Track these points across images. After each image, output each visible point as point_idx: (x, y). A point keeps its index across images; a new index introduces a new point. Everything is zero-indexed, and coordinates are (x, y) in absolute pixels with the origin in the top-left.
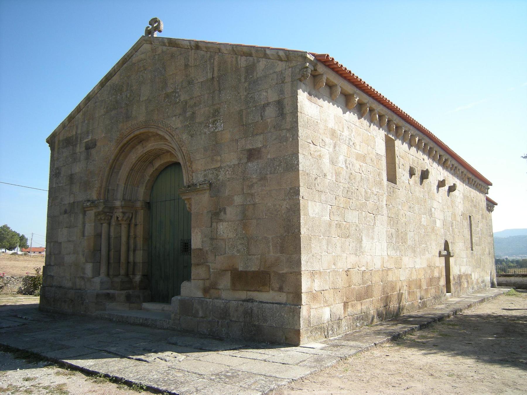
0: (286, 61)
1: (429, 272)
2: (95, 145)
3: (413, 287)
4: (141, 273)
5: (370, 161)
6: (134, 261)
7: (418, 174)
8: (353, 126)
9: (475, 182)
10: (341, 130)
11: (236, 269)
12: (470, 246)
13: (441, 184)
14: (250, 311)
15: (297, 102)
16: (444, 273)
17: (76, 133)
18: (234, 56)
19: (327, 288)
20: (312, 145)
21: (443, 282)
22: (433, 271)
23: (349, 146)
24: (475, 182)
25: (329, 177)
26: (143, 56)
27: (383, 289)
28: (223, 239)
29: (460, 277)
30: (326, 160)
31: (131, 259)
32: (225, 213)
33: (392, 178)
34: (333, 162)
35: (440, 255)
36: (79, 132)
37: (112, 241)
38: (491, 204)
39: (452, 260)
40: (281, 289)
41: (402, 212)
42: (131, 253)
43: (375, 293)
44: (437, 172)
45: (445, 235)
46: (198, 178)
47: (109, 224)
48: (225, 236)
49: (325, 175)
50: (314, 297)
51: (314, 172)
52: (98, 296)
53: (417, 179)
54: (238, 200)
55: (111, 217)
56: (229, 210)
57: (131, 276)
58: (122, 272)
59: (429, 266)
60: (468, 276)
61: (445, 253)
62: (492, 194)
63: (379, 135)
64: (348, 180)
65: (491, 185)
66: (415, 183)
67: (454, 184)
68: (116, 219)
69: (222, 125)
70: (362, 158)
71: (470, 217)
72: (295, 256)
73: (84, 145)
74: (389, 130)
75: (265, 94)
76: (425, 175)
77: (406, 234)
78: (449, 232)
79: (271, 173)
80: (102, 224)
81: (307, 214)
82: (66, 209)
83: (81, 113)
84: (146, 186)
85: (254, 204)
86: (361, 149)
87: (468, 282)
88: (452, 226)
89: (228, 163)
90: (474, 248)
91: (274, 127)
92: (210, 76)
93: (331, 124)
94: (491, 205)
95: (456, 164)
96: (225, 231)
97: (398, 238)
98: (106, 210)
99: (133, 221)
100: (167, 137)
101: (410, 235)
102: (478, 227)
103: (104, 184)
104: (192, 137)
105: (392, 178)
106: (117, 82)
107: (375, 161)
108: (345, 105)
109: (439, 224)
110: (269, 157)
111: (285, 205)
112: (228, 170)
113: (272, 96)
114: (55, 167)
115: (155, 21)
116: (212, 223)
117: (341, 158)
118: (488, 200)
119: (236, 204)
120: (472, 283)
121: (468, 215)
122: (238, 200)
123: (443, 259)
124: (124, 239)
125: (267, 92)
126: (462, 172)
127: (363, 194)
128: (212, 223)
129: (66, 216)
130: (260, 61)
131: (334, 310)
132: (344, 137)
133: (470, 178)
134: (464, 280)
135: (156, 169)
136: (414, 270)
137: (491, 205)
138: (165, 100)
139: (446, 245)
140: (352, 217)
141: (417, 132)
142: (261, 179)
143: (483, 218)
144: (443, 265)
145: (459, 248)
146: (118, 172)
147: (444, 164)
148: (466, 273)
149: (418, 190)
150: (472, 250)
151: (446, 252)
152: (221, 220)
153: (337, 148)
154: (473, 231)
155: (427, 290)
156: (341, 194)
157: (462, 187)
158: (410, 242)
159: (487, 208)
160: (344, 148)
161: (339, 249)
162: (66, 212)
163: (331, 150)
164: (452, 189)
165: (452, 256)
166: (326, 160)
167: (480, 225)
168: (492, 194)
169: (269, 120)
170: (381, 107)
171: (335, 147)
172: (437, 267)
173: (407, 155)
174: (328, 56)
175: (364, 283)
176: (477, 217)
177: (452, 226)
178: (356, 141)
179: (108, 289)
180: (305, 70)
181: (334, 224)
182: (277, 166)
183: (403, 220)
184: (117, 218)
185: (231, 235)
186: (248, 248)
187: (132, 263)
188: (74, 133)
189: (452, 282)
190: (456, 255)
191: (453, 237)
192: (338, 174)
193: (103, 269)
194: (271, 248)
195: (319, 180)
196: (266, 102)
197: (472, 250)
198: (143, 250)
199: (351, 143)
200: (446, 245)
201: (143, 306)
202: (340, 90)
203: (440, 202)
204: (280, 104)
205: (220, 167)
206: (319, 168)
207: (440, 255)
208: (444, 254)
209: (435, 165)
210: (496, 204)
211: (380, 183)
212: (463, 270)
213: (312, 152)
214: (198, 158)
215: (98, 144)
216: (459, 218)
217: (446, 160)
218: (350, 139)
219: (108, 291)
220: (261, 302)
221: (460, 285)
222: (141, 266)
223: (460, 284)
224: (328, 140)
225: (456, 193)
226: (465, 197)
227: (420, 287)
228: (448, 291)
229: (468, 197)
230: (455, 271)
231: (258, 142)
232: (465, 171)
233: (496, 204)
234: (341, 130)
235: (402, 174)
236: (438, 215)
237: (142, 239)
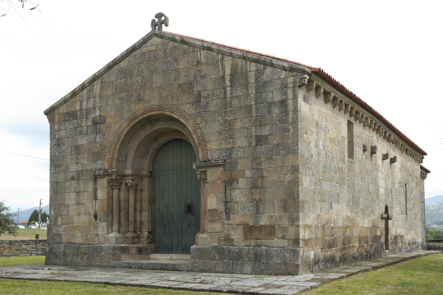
0: (289, 71)
1: (373, 231)
2: (104, 122)
3: (362, 242)
4: (147, 230)
5: (337, 143)
6: (140, 220)
7: (369, 150)
8: (328, 116)
9: (412, 152)
10: (321, 120)
11: (248, 224)
12: (405, 210)
13: (385, 157)
14: (259, 253)
15: (297, 103)
16: (384, 233)
17: (80, 108)
18: (244, 61)
19: (312, 237)
20: (305, 135)
21: (383, 240)
22: (376, 231)
23: (326, 133)
24: (412, 152)
25: (314, 157)
26: (153, 48)
27: (344, 241)
28: (236, 202)
29: (396, 237)
30: (313, 145)
31: (138, 218)
33: (351, 154)
34: (316, 146)
35: (382, 218)
36: (84, 107)
37: (122, 203)
38: (425, 172)
39: (390, 222)
40: (283, 238)
41: (356, 182)
42: (138, 214)
43: (338, 244)
44: (383, 147)
45: (386, 200)
46: (213, 155)
47: (119, 189)
48: (238, 200)
49: (312, 156)
50: (306, 242)
51: (307, 154)
52: (114, 248)
53: (367, 154)
54: (248, 173)
55: (121, 183)
56: (240, 180)
57: (139, 233)
58: (131, 229)
59: (374, 226)
60: (402, 237)
61: (385, 216)
62: (426, 163)
63: (342, 121)
64: (325, 159)
65: (426, 154)
66: (366, 157)
67: (395, 157)
68: (125, 185)
69: (234, 115)
70: (332, 140)
71: (406, 184)
72: (295, 214)
73: (91, 120)
74: (351, 115)
75: (271, 94)
76: (373, 151)
77: (359, 200)
78: (389, 198)
79: (276, 155)
80: (113, 189)
81: (302, 185)
82: (73, 176)
83: (85, 91)
84: (150, 158)
85: (262, 177)
86: (332, 134)
87: (402, 242)
88: (391, 193)
89: (240, 145)
90: (408, 213)
91: (279, 121)
92: (221, 73)
93: (316, 117)
94: (425, 172)
95: (397, 138)
96: (238, 196)
97: (354, 203)
98: (118, 178)
99: (139, 187)
100: (183, 121)
101: (362, 200)
102: (412, 194)
103: (116, 156)
104: (206, 122)
105: (351, 154)
106: (125, 67)
107: (341, 143)
108: (323, 100)
109: (382, 191)
110: (274, 142)
111: (287, 178)
112: (239, 151)
113: (277, 97)
114: (57, 137)
115: (159, 16)
116: (226, 190)
117: (321, 142)
118: (422, 168)
119: (247, 176)
120: (406, 244)
121: (404, 183)
122: (248, 173)
123: (383, 222)
124: (132, 202)
125: (272, 93)
126: (402, 145)
127: (333, 168)
128: (226, 190)
129: (73, 182)
130: (266, 68)
131: (316, 253)
132: (323, 126)
133: (408, 149)
134: (399, 240)
135: (160, 144)
136: (363, 228)
137: (425, 172)
138: (178, 90)
139: (387, 208)
140: (326, 186)
141: (370, 115)
142: (268, 159)
143: (417, 186)
144: (384, 226)
145: (396, 212)
146: (127, 145)
147: (388, 139)
148: (401, 234)
149: (368, 164)
150: (406, 214)
151: (386, 215)
152: (235, 189)
153: (319, 135)
154: (408, 197)
155: (371, 246)
156: (320, 170)
157: (401, 158)
158: (361, 206)
159: (421, 176)
160: (323, 133)
161: (319, 210)
162: (73, 178)
163: (316, 137)
164: (393, 160)
165: (391, 219)
166: (313, 145)
167: (414, 192)
168: (426, 163)
169: (275, 115)
170: (347, 99)
171: (317, 134)
172: (379, 227)
173: (364, 135)
174: (320, 68)
175: (332, 236)
176: (412, 185)
177: (391, 193)
178: (330, 128)
179: (121, 243)
180: (304, 80)
181: (317, 191)
182: (281, 150)
183: (357, 188)
184: (126, 184)
185: (243, 199)
186: (257, 209)
187: (139, 222)
188: (78, 108)
189: (390, 241)
190: (393, 219)
191: (392, 202)
192: (319, 154)
193: (115, 227)
194: (276, 208)
195: (309, 160)
196: (272, 101)
197: (406, 214)
198: (148, 211)
199: (327, 130)
200: (387, 208)
201: (151, 257)
202: (322, 90)
203: (383, 172)
204: (283, 103)
205: (233, 148)
206: (309, 151)
207: (382, 218)
208: (384, 216)
209: (381, 139)
210: (429, 172)
211: (343, 160)
212: (398, 232)
213: (305, 140)
214: (212, 140)
215: (108, 121)
216: (397, 186)
217: (390, 135)
218: (326, 127)
219: (123, 245)
220: (269, 247)
221: (396, 244)
222: (147, 224)
223: (396, 243)
224: (314, 130)
225: (396, 164)
226: (403, 167)
227: (367, 243)
228: (387, 249)
229: (405, 167)
230: (393, 231)
231: (266, 131)
232: (404, 143)
233: (429, 172)
234: (321, 120)
235: (358, 150)
236: (381, 183)
237: (147, 202)
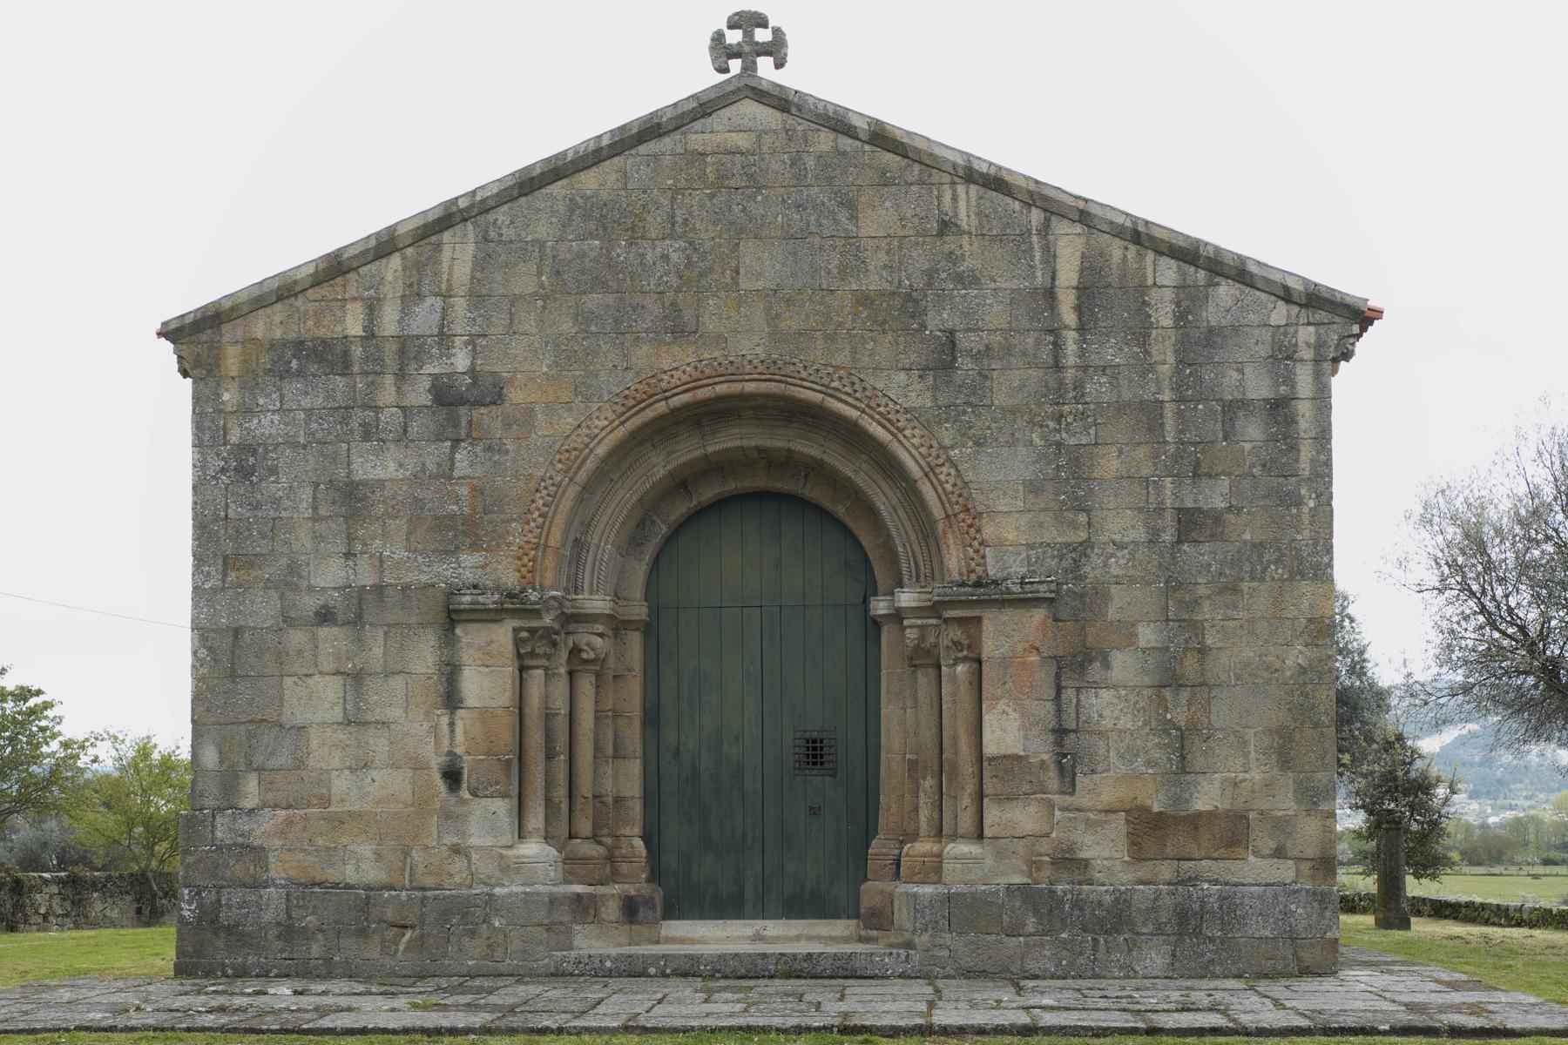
32: (1106, 665)
48: (1107, 723)
56: (1119, 659)
128: (1059, 689)
152: (1096, 686)
